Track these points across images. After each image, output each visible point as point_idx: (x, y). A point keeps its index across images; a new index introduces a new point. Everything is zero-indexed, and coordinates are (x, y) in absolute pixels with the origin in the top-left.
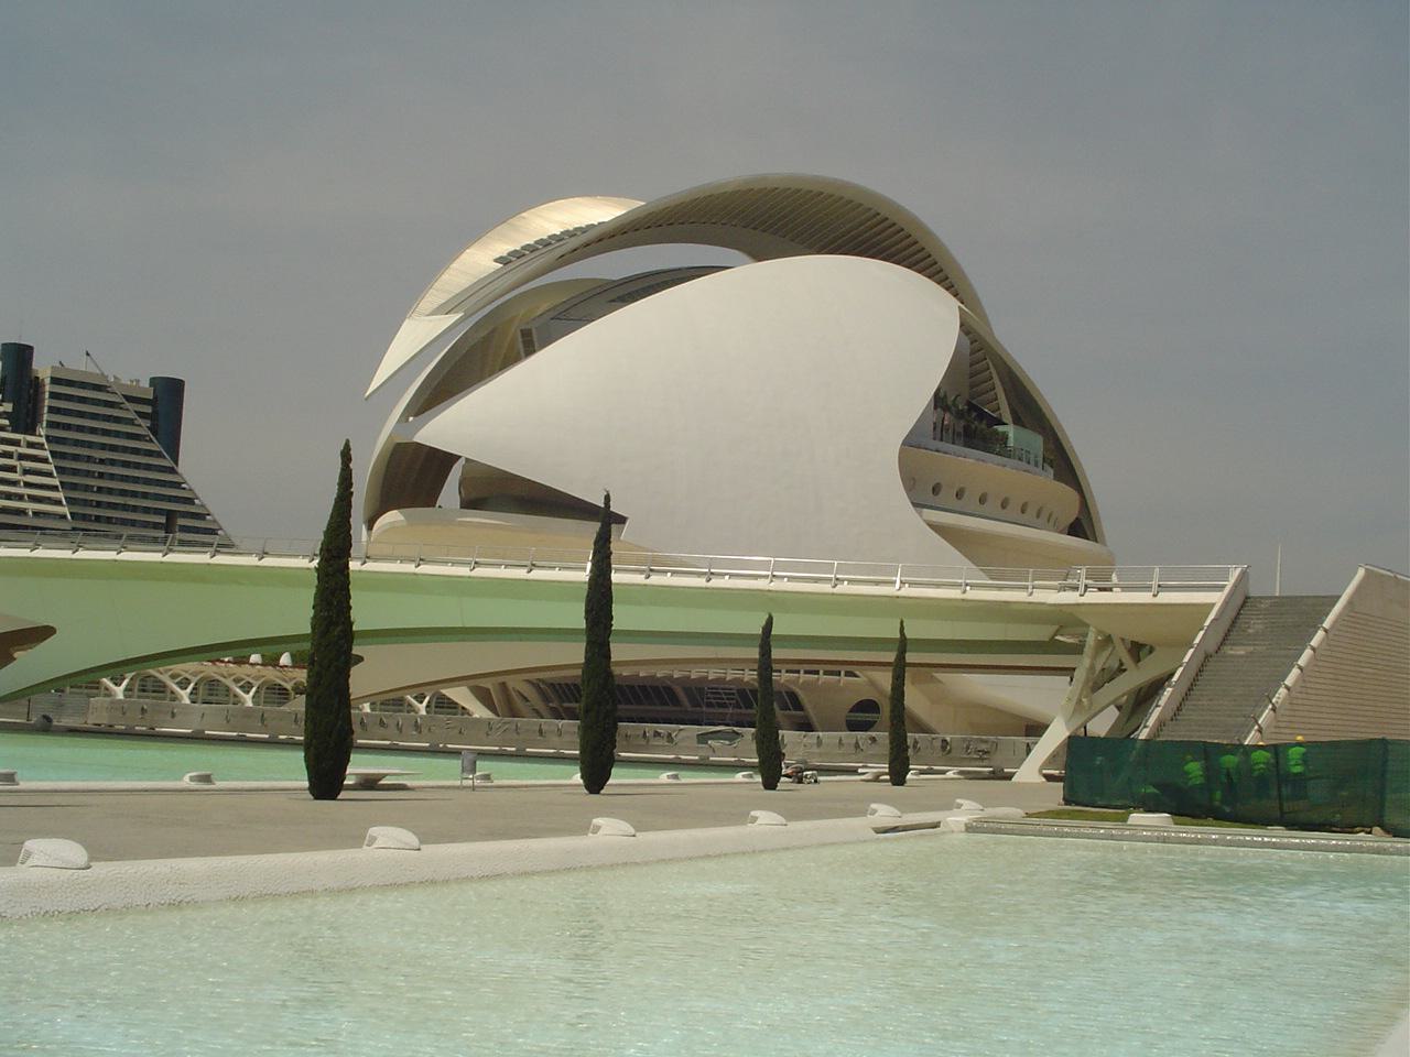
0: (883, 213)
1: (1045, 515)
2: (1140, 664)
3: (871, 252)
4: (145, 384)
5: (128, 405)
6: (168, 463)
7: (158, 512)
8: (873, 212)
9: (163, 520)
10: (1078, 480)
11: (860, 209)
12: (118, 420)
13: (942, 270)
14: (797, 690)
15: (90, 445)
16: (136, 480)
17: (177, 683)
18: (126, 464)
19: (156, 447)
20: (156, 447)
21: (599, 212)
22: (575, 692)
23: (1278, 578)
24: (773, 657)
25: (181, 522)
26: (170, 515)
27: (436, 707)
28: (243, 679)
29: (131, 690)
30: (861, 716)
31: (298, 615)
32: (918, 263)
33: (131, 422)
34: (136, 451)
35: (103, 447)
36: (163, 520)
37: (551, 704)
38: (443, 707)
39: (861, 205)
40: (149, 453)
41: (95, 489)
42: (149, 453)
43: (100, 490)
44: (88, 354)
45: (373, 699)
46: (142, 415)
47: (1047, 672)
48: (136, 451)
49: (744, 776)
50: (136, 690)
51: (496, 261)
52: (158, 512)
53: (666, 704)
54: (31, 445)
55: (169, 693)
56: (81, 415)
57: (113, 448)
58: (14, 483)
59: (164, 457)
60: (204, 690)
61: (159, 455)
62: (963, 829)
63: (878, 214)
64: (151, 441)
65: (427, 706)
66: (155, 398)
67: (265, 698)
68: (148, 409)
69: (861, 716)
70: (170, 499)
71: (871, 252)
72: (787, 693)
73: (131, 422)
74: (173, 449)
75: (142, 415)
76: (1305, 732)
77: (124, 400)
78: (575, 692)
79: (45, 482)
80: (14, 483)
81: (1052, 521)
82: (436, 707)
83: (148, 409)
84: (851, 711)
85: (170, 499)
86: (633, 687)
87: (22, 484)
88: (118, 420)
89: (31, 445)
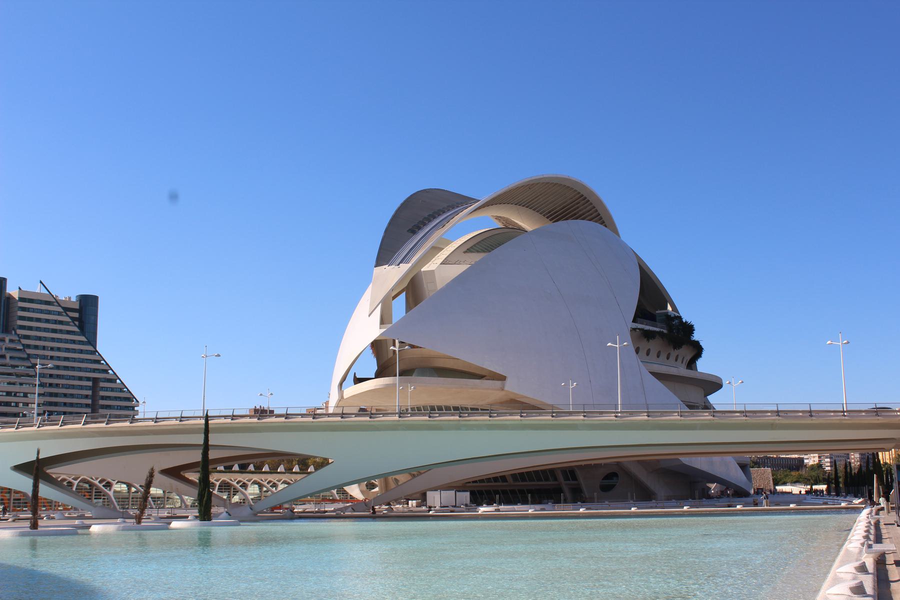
2: (889, 514)
3: (589, 218)
4: (74, 299)
6: (90, 348)
7: (88, 379)
8: (552, 221)
12: (61, 323)
16: (74, 360)
18: (68, 350)
23: (569, 474)
24: (210, 458)
25: (102, 384)
26: (95, 381)
30: (607, 482)
31: (201, 442)
32: (522, 204)
35: (53, 340)
36: (90, 384)
39: (550, 220)
41: (49, 358)
44: (218, 356)
46: (73, 319)
47: (366, 519)
52: (88, 379)
54: (11, 341)
56: (39, 320)
68: (76, 315)
69: (607, 482)
70: (94, 370)
71: (589, 218)
74: (92, 341)
83: (76, 315)
84: (603, 479)
85: (94, 370)
89: (11, 341)
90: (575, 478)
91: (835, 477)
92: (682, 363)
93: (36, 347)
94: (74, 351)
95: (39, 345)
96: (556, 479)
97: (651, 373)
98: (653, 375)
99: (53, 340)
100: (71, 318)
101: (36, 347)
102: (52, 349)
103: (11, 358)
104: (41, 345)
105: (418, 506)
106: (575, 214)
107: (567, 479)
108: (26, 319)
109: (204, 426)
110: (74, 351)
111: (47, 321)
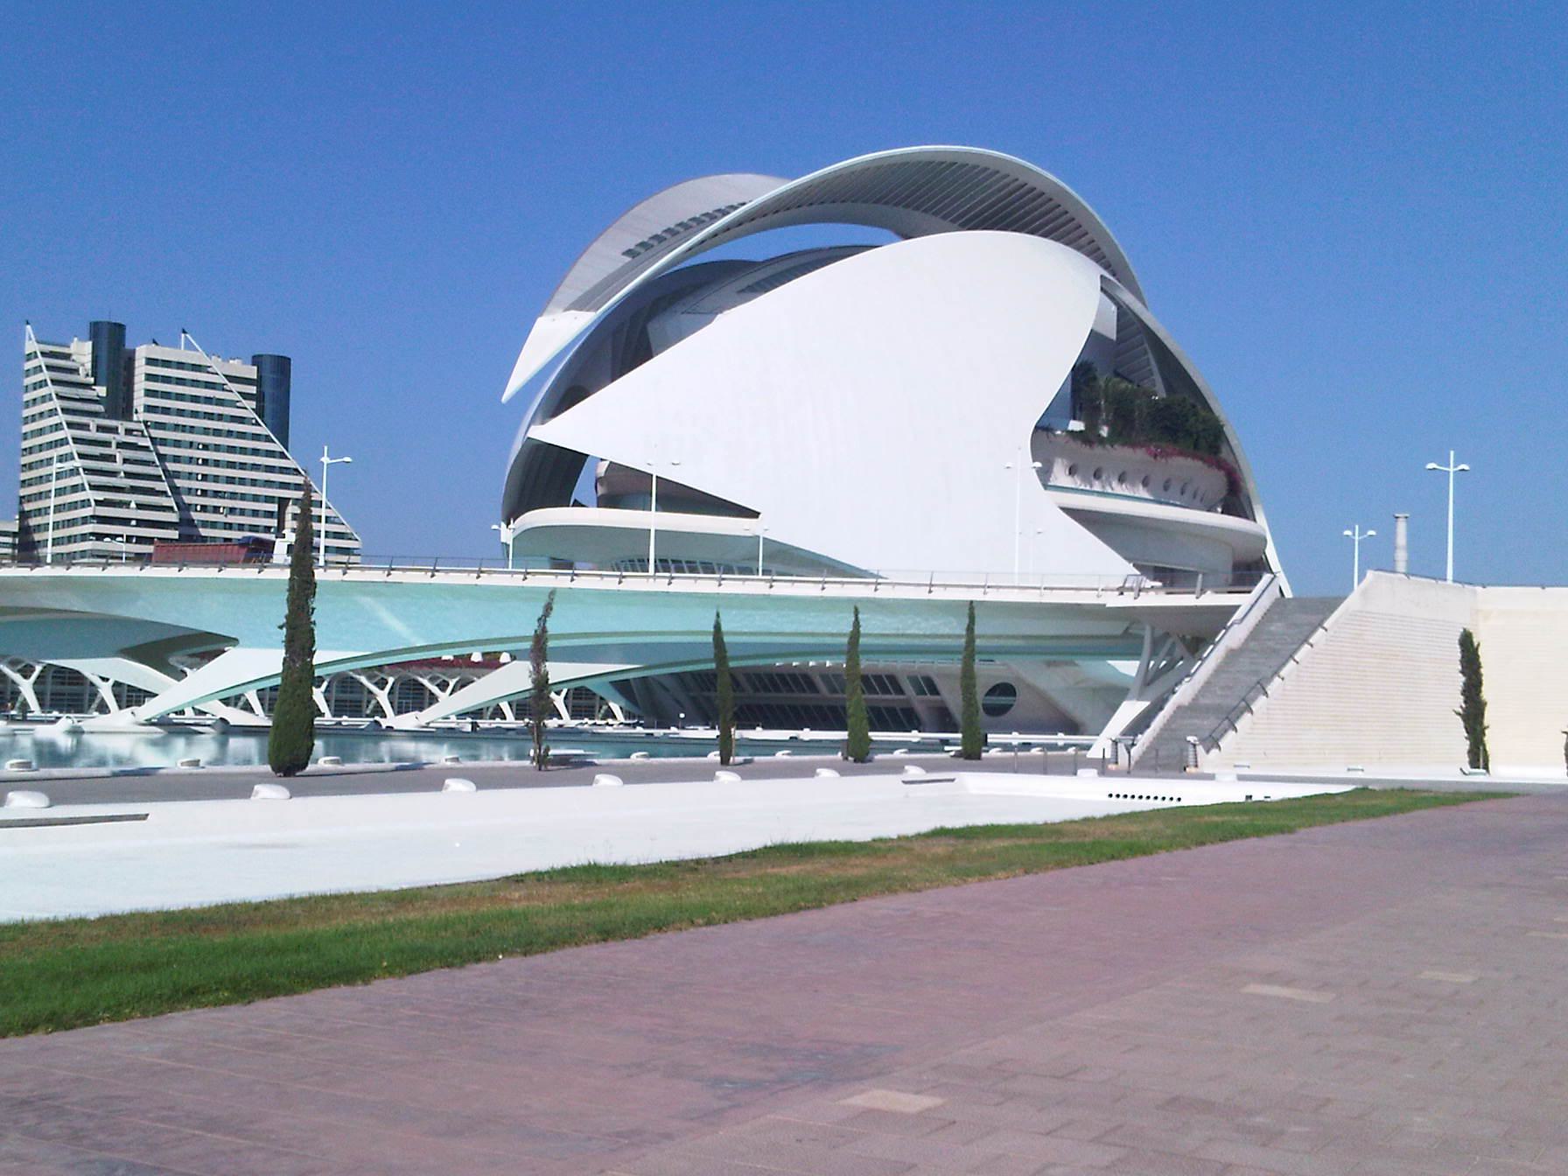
0: (1040, 188)
1: (1190, 490)
5: (231, 386)
7: (269, 499)
9: (274, 507)
10: (800, 223)
11: (1035, 192)
12: (220, 402)
13: (1099, 249)
14: (810, 673)
15: (192, 429)
17: (438, 685)
19: (263, 430)
20: (263, 430)
21: (761, 189)
22: (59, 675)
27: (360, 702)
28: (438, 678)
29: (329, 691)
30: (1003, 700)
33: (232, 404)
34: (242, 435)
36: (274, 507)
37: (692, 694)
38: (581, 698)
40: (256, 437)
42: (256, 437)
43: (205, 477)
45: (511, 699)
46: (245, 396)
48: (242, 435)
49: (901, 753)
50: (334, 691)
51: (624, 254)
52: (269, 499)
53: (804, 691)
54: (129, 432)
55: (366, 693)
57: (217, 432)
58: (113, 474)
59: (274, 442)
60: (337, 687)
61: (268, 439)
62: (1217, 776)
63: (1066, 212)
64: (257, 424)
65: (565, 698)
66: (260, 376)
67: (400, 693)
68: (253, 390)
69: (1003, 700)
72: (886, 676)
73: (232, 404)
75: (245, 396)
76: (356, 732)
77: (226, 382)
78: (59, 675)
79: (140, 467)
80: (113, 474)
81: (1198, 498)
82: (574, 698)
83: (253, 390)
86: (880, 677)
87: (122, 474)
88: (220, 402)
89: (129, 432)
90: (934, 690)
91: (974, 655)
92: (1182, 493)
93: (177, 444)
94: (243, 451)
95: (167, 422)
96: (900, 691)
97: (1063, 509)
98: (1067, 513)
99: (231, 465)
100: (152, 439)
101: (177, 444)
102: (206, 447)
103: (125, 461)
104: (187, 439)
105: (470, 655)
106: (976, 216)
107: (921, 692)
108: (173, 396)
109: (710, 639)
110: (243, 451)
111: (254, 482)
